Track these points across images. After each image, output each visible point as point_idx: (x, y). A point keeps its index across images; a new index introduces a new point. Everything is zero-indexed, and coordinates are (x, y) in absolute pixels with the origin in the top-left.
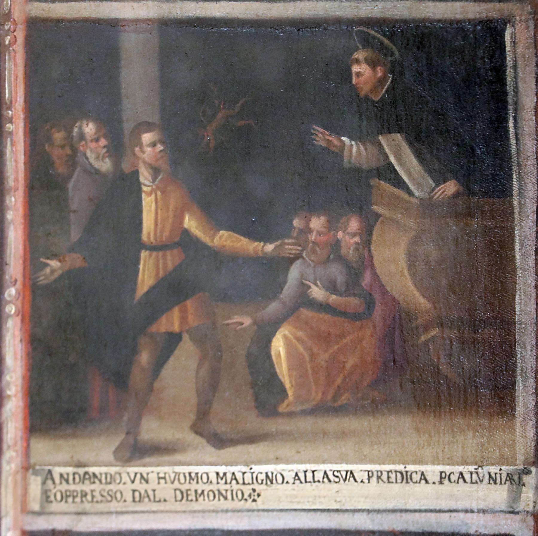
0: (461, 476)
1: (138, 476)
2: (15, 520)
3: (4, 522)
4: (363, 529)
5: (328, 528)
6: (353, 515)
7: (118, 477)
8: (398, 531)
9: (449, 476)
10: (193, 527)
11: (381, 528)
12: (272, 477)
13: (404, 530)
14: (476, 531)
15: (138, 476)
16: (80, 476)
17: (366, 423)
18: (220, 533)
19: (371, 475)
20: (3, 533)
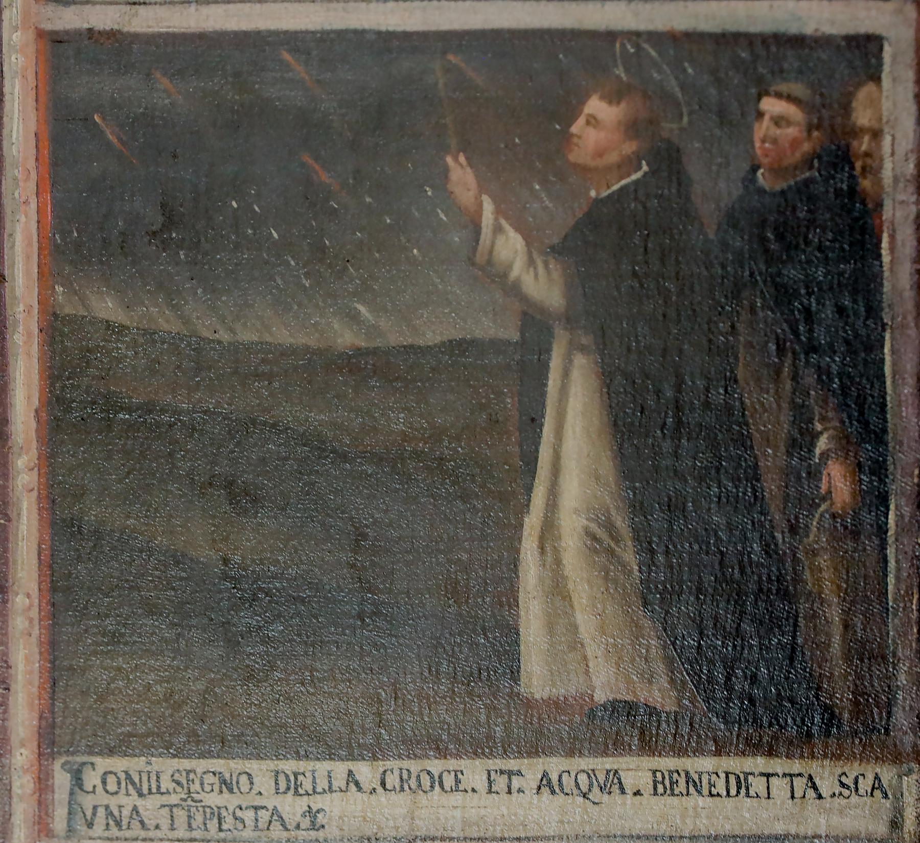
0: (810, 784)
1: (101, 812)
2: (26, 14)
3: (6, 15)
4: (619, 28)
5: (560, 27)
6: (603, 6)
7: (244, 779)
8: (681, 32)
9: (440, 777)
10: (327, 27)
11: (651, 27)
12: (231, 779)
13: (691, 30)
14: (816, 30)
15: (101, 812)
16: (287, 776)
17: (697, 145)
18: (374, 37)
19: (405, 776)
20: (895, 26)
